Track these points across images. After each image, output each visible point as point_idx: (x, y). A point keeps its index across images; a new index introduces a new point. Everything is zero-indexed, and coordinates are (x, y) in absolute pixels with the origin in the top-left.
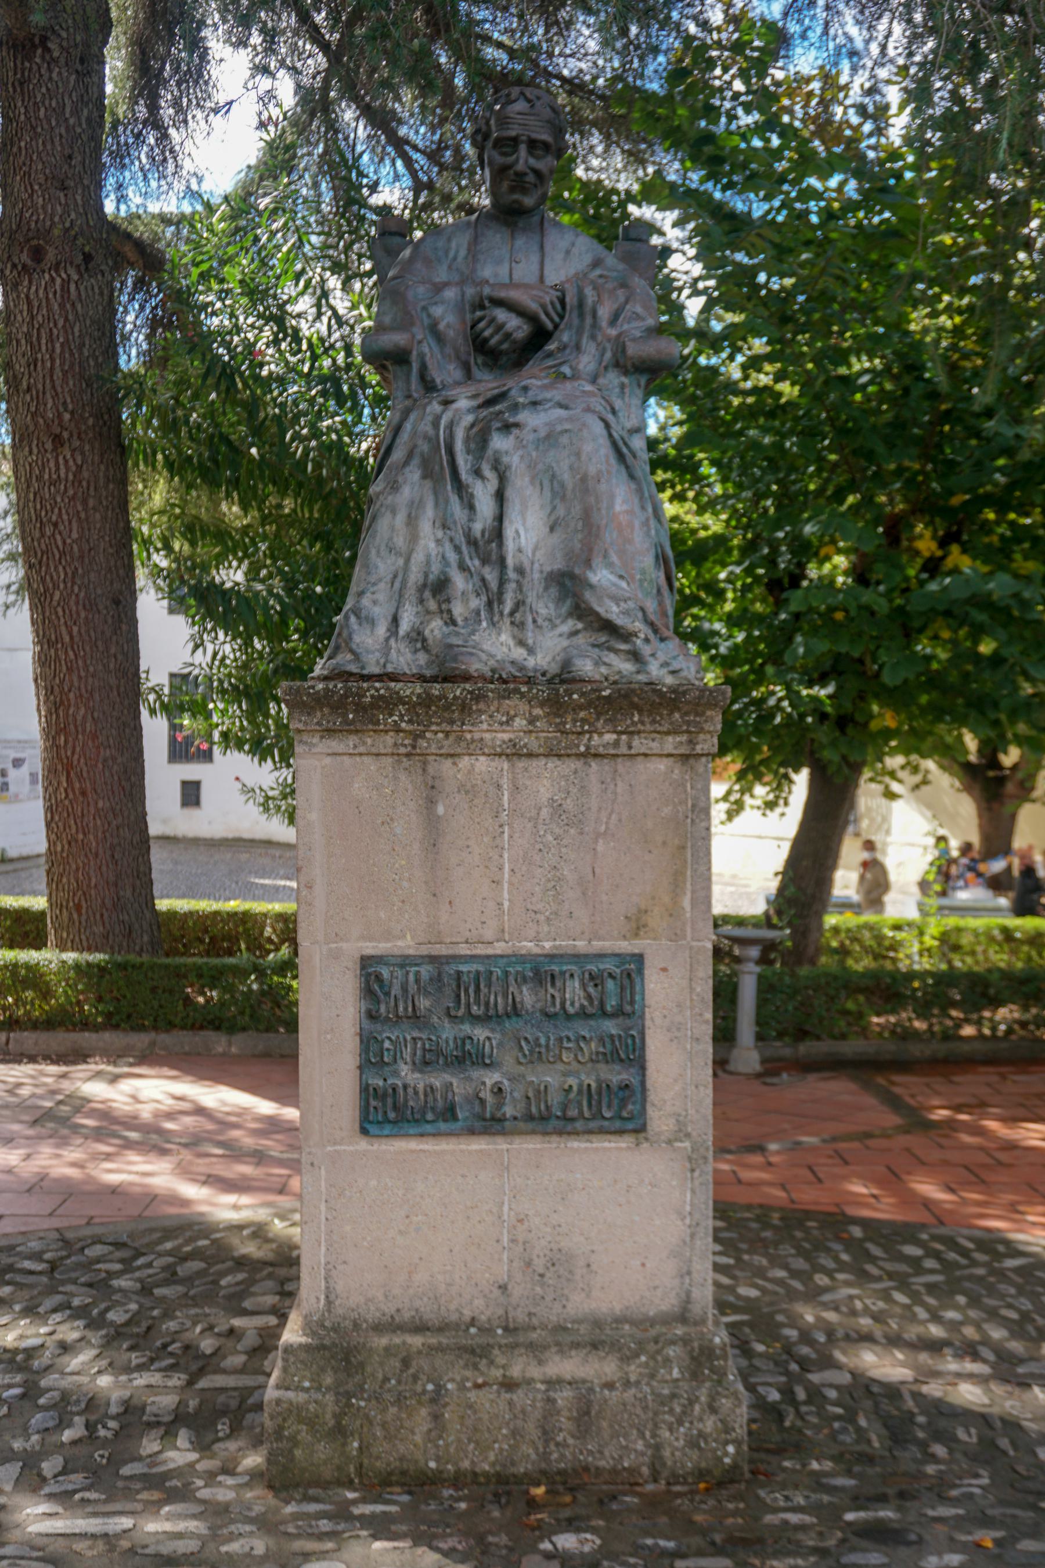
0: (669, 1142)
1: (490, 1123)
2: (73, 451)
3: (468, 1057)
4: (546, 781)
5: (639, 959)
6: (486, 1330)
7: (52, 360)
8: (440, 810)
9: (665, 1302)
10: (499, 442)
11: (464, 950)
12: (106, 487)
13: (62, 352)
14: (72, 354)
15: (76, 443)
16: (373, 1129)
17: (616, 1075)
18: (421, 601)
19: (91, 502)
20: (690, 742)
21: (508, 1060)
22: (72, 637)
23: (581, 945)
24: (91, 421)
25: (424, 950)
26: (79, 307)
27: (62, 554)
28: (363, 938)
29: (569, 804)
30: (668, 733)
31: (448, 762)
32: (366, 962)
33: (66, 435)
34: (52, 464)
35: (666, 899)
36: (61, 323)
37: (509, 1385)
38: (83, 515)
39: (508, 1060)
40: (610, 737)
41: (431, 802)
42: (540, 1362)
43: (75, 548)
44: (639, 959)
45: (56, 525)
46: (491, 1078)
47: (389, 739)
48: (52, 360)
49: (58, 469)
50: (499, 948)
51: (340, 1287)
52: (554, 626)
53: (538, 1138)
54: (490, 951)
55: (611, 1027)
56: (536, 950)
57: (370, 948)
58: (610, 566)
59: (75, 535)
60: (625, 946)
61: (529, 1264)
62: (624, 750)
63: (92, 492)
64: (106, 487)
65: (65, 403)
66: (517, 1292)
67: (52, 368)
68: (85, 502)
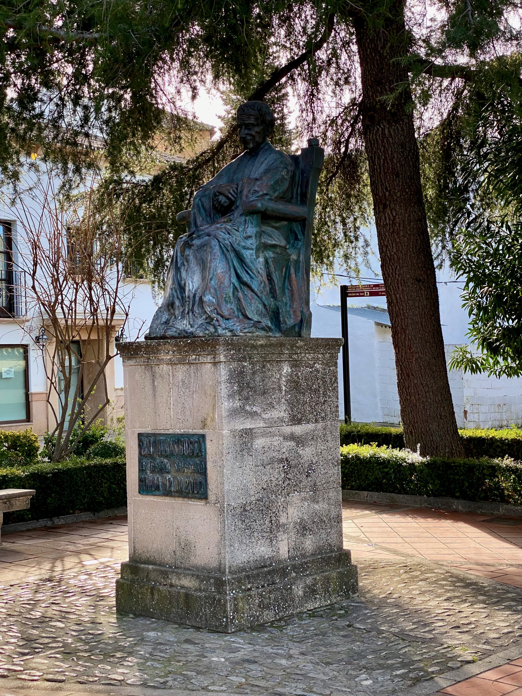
0: (214, 504)
1: (168, 493)
2: (391, 211)
3: (162, 470)
4: (181, 372)
5: (203, 436)
6: (170, 567)
7: (380, 167)
8: (156, 384)
9: (214, 564)
10: (187, 252)
11: (162, 432)
12: (410, 225)
13: (384, 164)
14: (388, 164)
15: (393, 206)
16: (143, 491)
17: (199, 478)
18: (169, 310)
19: (401, 234)
20: (214, 358)
21: (173, 471)
22: (397, 299)
23: (191, 431)
24: (398, 195)
25: (153, 432)
26: (391, 140)
27: (390, 260)
28: (139, 428)
29: (186, 381)
30: (208, 355)
31: (157, 367)
32: (140, 435)
33: (388, 203)
34: (383, 218)
35: (211, 415)
36: (382, 149)
37: (171, 586)
38: (398, 240)
39: (173, 471)
40: (194, 357)
41: (154, 381)
42: (179, 579)
43: (396, 257)
44: (203, 436)
45: (387, 247)
46: (169, 476)
47: (142, 359)
48: (380, 167)
49: (386, 219)
50: (171, 431)
51: (137, 547)
52: (201, 317)
53: (181, 499)
54: (168, 433)
55: (197, 460)
56: (179, 433)
57: (142, 431)
58: (211, 293)
59: (395, 251)
60: (201, 432)
61: (180, 544)
62: (197, 362)
63: (401, 228)
64: (410, 225)
65: (386, 188)
66: (178, 553)
67: (380, 172)
68: (398, 234)
